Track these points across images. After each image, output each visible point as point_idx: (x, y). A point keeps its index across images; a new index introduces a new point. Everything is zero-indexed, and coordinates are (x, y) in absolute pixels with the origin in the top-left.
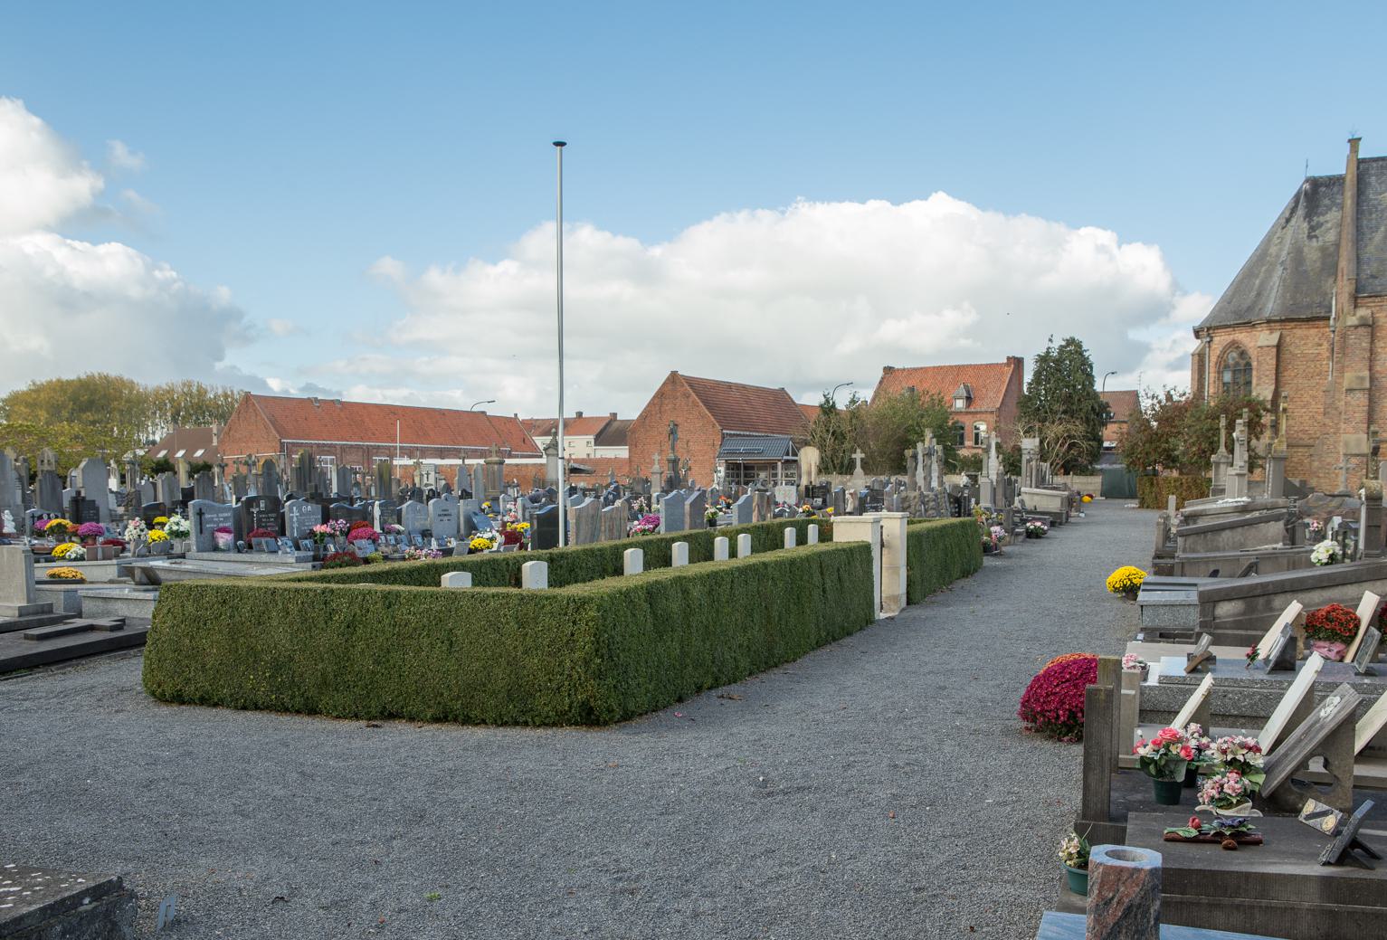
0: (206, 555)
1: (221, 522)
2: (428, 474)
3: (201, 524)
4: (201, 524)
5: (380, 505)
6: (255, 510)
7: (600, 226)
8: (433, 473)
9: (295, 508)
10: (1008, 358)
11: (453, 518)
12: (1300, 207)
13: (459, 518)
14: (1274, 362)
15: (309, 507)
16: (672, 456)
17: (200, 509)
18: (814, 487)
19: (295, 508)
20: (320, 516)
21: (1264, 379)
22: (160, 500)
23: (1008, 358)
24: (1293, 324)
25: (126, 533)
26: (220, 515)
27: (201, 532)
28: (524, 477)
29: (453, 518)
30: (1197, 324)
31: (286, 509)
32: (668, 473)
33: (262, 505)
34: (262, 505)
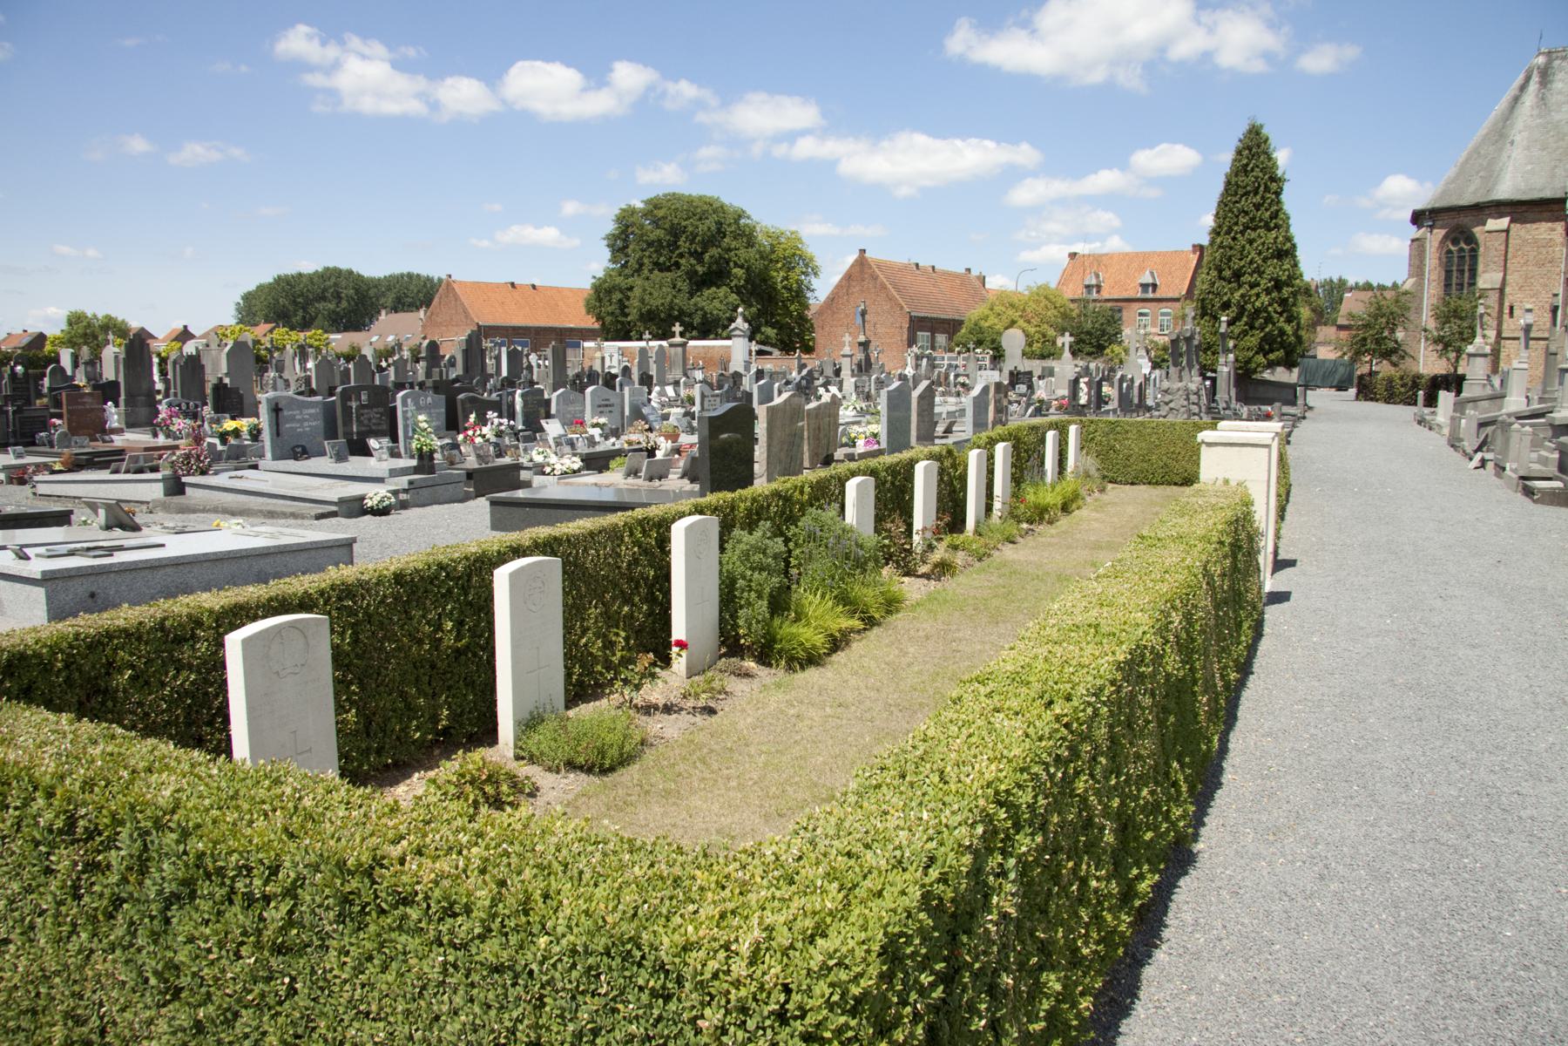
0: (291, 465)
1: (306, 420)
2: (611, 356)
3: (278, 425)
4: (278, 425)
5: (523, 396)
6: (354, 405)
7: (692, 81)
8: (616, 355)
9: (409, 400)
10: (1194, 246)
11: (616, 410)
12: (1532, 82)
13: (623, 408)
14: (1503, 248)
15: (429, 399)
16: (862, 338)
17: (277, 404)
18: (1019, 373)
19: (409, 400)
20: (443, 410)
21: (1492, 266)
22: (1266, 437)
23: (1194, 246)
24: (1524, 208)
25: (237, 1024)
26: (305, 411)
27: (278, 434)
28: (711, 359)
29: (616, 410)
30: (1419, 206)
31: (399, 403)
32: (860, 356)
33: (364, 397)
34: (364, 397)
